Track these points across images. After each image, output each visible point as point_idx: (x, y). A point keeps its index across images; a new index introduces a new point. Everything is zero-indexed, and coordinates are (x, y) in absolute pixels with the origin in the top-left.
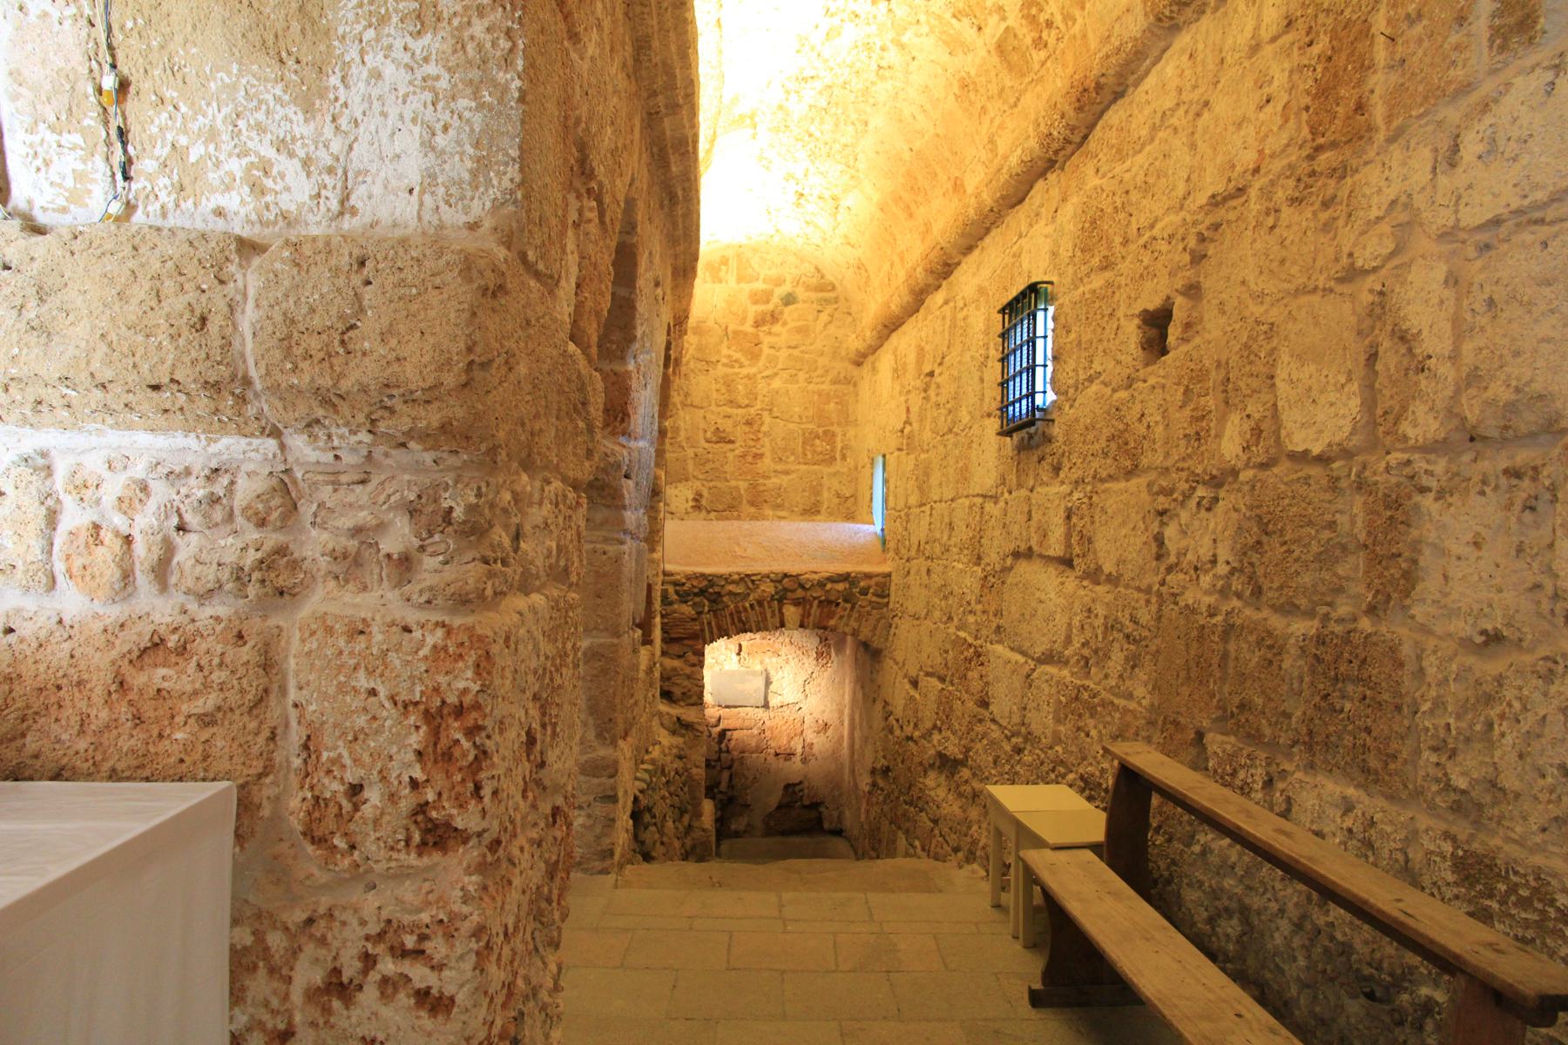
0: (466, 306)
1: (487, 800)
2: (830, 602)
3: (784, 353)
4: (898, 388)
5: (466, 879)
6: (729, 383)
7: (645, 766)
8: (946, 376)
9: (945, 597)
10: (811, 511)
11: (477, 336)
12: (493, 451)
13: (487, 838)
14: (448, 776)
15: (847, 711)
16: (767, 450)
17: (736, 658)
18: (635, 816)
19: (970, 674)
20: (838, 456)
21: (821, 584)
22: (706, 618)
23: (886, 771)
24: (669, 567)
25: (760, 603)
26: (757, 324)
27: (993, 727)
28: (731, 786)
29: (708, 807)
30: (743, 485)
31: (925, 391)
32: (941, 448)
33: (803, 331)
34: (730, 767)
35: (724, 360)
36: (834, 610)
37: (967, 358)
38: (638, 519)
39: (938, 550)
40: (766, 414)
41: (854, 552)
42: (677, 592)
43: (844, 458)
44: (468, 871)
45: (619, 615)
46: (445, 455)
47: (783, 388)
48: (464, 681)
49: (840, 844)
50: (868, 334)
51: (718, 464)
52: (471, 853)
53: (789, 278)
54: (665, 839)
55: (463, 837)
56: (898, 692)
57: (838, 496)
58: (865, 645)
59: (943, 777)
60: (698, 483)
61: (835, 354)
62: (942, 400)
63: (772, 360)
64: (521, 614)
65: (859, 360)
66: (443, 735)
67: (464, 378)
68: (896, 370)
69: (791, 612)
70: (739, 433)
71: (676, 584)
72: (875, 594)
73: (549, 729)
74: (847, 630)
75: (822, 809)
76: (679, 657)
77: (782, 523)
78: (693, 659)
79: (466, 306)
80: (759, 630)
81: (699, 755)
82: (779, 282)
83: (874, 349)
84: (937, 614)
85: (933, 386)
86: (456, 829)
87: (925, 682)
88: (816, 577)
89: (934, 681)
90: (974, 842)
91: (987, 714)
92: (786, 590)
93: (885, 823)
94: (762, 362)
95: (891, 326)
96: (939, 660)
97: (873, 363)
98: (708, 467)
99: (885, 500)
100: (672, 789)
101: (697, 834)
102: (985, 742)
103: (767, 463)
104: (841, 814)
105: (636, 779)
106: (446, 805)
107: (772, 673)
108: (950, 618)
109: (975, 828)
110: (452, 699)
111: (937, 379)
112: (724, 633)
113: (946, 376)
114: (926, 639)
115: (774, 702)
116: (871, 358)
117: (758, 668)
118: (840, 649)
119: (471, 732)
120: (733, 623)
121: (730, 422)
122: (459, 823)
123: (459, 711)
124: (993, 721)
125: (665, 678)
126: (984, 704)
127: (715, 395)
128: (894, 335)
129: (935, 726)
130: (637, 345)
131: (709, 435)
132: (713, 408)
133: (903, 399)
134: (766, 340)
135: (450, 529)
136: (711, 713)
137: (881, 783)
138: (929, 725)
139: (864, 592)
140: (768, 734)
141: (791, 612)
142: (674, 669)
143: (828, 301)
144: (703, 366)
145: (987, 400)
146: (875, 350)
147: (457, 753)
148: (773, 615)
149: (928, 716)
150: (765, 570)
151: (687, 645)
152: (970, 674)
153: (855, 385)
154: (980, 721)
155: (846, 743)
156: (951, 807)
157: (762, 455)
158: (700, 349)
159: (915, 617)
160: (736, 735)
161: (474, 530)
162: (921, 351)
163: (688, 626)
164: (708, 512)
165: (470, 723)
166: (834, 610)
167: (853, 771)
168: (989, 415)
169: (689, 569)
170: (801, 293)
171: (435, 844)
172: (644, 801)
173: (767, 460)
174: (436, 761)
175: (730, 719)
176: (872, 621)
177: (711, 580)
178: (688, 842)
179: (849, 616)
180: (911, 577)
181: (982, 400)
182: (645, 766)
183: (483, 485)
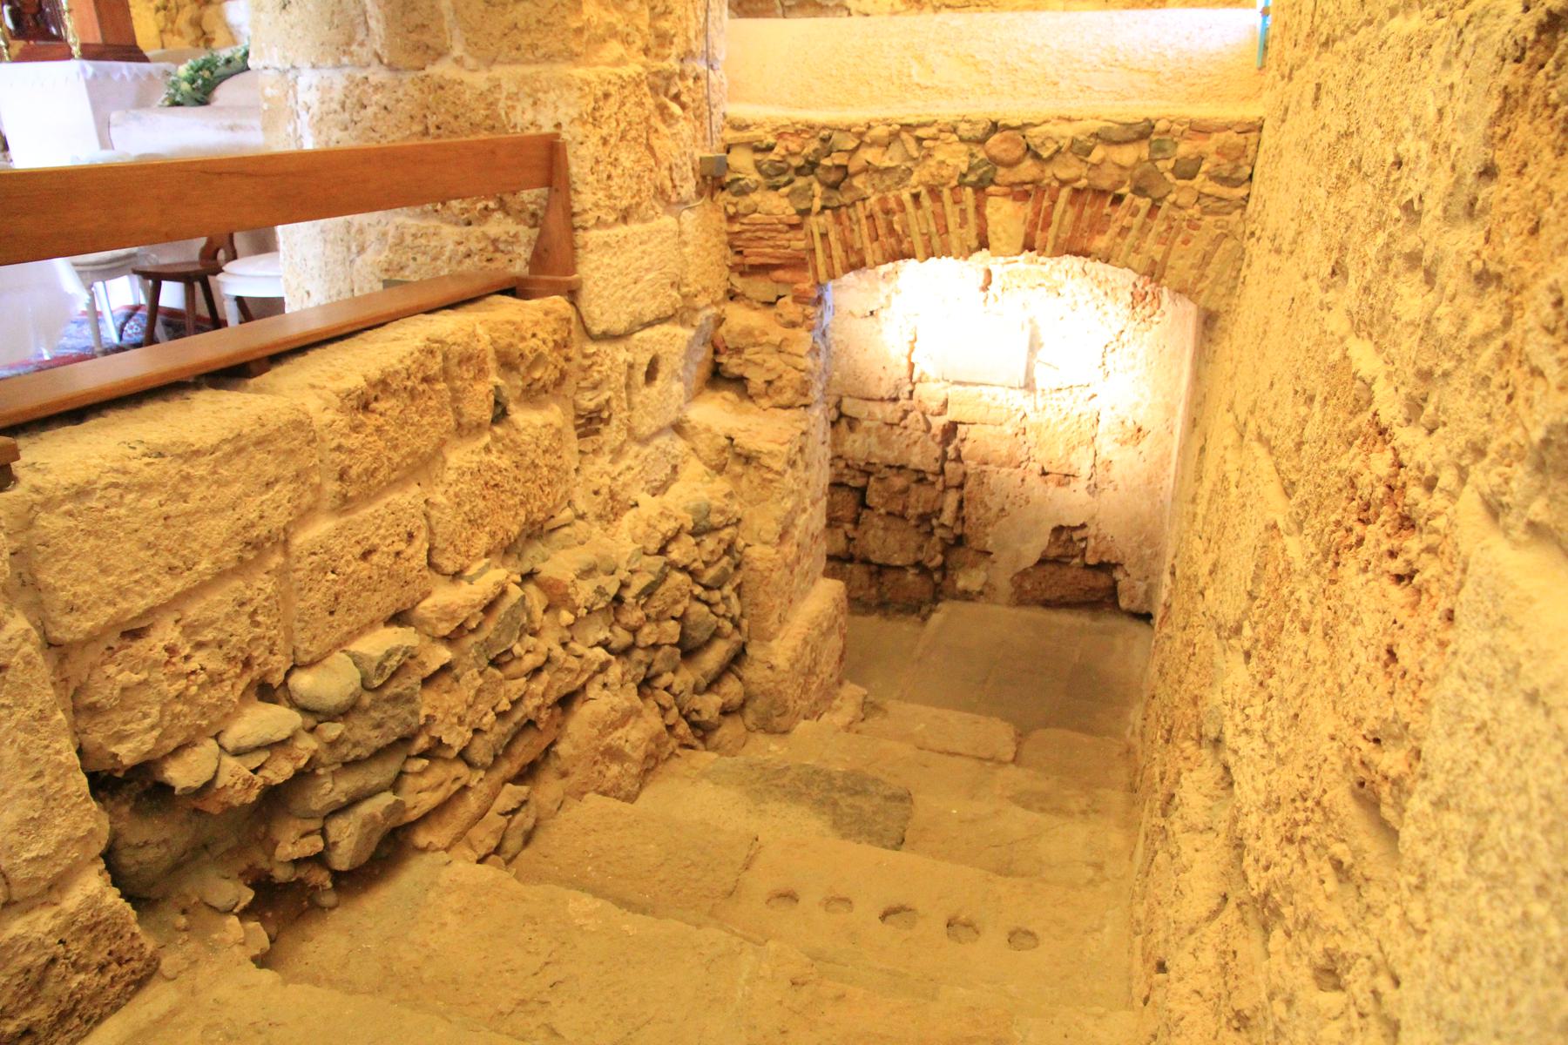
21: (1080, 150)
22: (816, 223)
28: (960, 518)
34: (960, 486)
69: (1004, 214)
75: (1118, 575)
80: (930, 254)
88: (1069, 131)
92: (994, 162)
115: (1042, 379)
120: (875, 238)
139: (1187, 171)
140: (1031, 435)
142: (748, 332)
148: (963, 223)
150: (946, 111)
155: (1172, 470)
163: (782, 240)
176: (1200, 243)
179: (1144, 230)
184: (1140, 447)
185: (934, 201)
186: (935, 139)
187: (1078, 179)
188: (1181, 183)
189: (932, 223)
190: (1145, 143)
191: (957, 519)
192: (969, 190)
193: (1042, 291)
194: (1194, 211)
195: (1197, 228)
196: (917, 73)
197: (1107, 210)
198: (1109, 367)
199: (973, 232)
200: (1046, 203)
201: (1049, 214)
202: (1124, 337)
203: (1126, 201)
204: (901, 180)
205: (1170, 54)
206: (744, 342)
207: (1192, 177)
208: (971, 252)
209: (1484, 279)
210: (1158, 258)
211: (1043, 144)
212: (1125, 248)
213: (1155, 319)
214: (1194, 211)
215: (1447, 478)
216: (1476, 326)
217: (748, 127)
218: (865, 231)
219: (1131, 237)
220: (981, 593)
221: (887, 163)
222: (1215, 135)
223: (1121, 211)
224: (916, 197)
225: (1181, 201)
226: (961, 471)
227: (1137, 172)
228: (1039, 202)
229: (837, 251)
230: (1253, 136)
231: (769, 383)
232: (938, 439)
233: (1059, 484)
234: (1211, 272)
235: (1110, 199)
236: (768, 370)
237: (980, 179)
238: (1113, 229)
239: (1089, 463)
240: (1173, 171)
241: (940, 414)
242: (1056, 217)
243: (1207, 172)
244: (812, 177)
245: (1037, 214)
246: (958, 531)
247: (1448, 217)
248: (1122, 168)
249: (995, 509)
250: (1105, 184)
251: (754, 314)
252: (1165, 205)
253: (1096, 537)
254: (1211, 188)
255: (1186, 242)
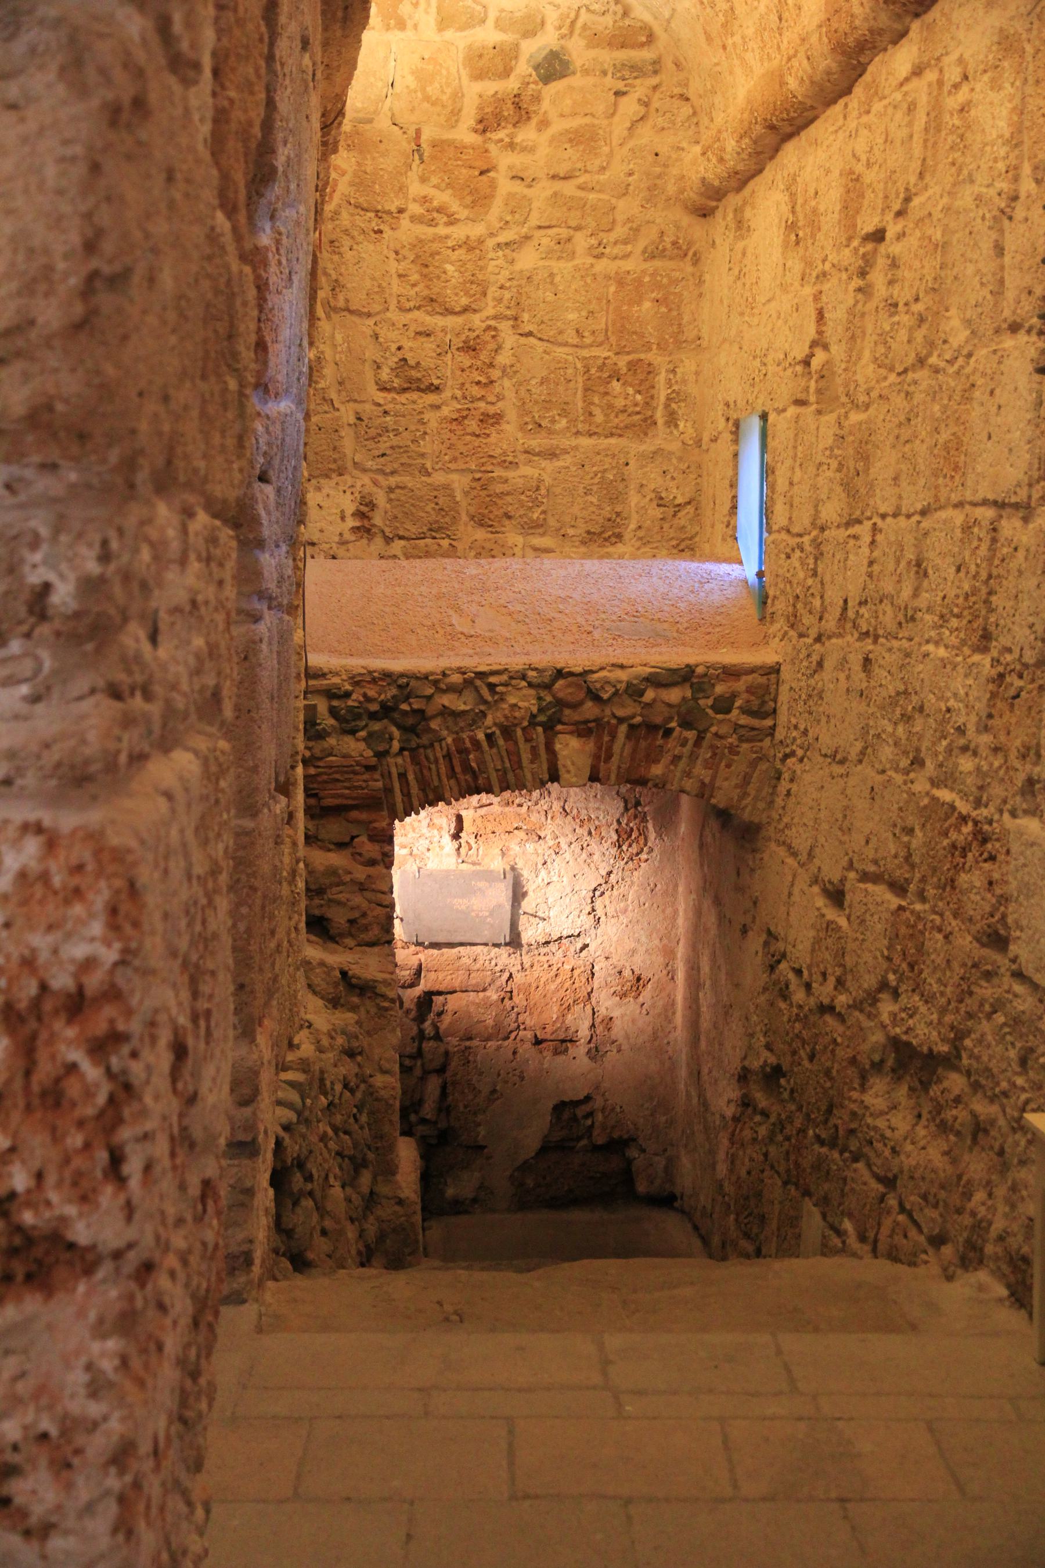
0: (78, 149)
1: (134, 1183)
2: (652, 728)
3: (541, 192)
4: (797, 266)
5: (96, 1347)
6: (425, 260)
7: (290, 1076)
8: (913, 241)
9: (907, 718)
10: (604, 536)
11: (104, 217)
12: (129, 464)
13: (133, 1258)
14: (56, 1136)
15: (681, 951)
16: (509, 407)
17: (449, 845)
18: (278, 1179)
19: (963, 878)
20: (660, 416)
21: (634, 691)
22: (395, 763)
23: (774, 1075)
24: (317, 660)
25: (507, 732)
26: (484, 126)
27: (1018, 988)
28: (444, 1107)
29: (407, 1154)
30: (459, 482)
31: (863, 274)
32: (898, 401)
33: (583, 139)
34: (441, 1070)
35: (415, 208)
36: (658, 746)
37: (966, 198)
38: (280, 566)
39: (888, 617)
40: (505, 326)
41: (700, 623)
42: (333, 712)
43: (672, 420)
44: (100, 1330)
45: (255, 769)
46: (29, 473)
47: (539, 267)
48: (84, 944)
49: (672, 1226)
50: (731, 144)
51: (405, 439)
52: (103, 1293)
53: (552, 17)
54: (328, 1223)
55: (85, 1260)
56: (801, 917)
57: (661, 502)
58: (724, 816)
59: (903, 1090)
60: (366, 479)
61: (653, 192)
62: (902, 294)
63: (517, 206)
64: (169, 796)
65: (707, 204)
66: (42, 1055)
67: (78, 309)
68: (791, 227)
69: (571, 749)
70: (450, 369)
71: (330, 694)
72: (746, 711)
73: (202, 1023)
74: (689, 784)
75: (633, 1153)
76: (341, 846)
77: (547, 563)
78: (371, 850)
79: (78, 149)
80: (505, 787)
81: (388, 1047)
82: (532, 26)
83: (740, 181)
84: (887, 752)
85: (881, 262)
86: (71, 1246)
87: (857, 892)
88: (623, 675)
89: (880, 892)
90: (980, 1227)
91: (1003, 962)
92: (561, 703)
93: (774, 1188)
94: (496, 209)
95: (783, 126)
96: (892, 848)
97: (738, 211)
98: (384, 446)
99: (766, 511)
100: (338, 1119)
101: (386, 1211)
102: (1000, 1018)
103: (510, 435)
104: (671, 1165)
105: (279, 1103)
106: (54, 1196)
107: (525, 873)
108: (918, 762)
109: (980, 1196)
110: (62, 981)
111: (891, 247)
112: (432, 796)
113: (913, 241)
114: (861, 804)
115: (530, 933)
116: (733, 200)
117: (497, 864)
118: (666, 822)
119: (99, 1048)
120: (452, 774)
121: (429, 346)
122: (81, 1233)
123: (76, 1005)
124: (1019, 975)
125: (314, 891)
126: (998, 940)
127: (396, 287)
128: (790, 147)
129: (884, 986)
130: (276, 190)
131: (385, 374)
132: (393, 315)
133: (808, 290)
134: (506, 161)
135: (44, 630)
136: (406, 957)
137: (762, 1100)
138: (870, 981)
139: (724, 706)
140: (519, 999)
141: (571, 749)
142: (332, 871)
143: (636, 70)
144: (366, 221)
145: (1010, 295)
146: (744, 183)
147: (73, 1088)
149: (869, 961)
150: (516, 662)
151: (356, 817)
152: (963, 878)
153: (696, 261)
154: (988, 975)
155: (679, 1019)
156: (924, 1152)
157: (497, 418)
158: (361, 182)
159: (836, 757)
160: (453, 1003)
161: (91, 630)
162: (854, 186)
164: (388, 540)
165: (99, 1026)
166: (658, 746)
167: (696, 1075)
168: (1014, 328)
169: (357, 663)
170: (578, 52)
171: (29, 1277)
172: (293, 1148)
173: (510, 427)
174: (29, 1108)
175: (441, 970)
176: (740, 766)
177: (404, 684)
178: (371, 1228)
179: (693, 757)
180: (827, 674)
181: (998, 292)
182: (290, 1076)
183: (112, 534)
184: (641, 999)
185: (506, 740)
186: (506, 685)
187: (633, 717)
188: (720, 717)
189: (507, 761)
190: (688, 685)
191: (440, 1110)
192: (540, 729)
193: (521, 834)
194: (732, 740)
195: (737, 753)
196: (460, 624)
197: (660, 742)
198: (600, 912)
199: (545, 767)
200: (606, 738)
201: (609, 749)
202: (613, 878)
203: (675, 734)
204: (474, 722)
205: (682, 605)
206: (327, 881)
207: (728, 711)
208: (543, 784)
209: (996, 750)
210: (707, 780)
211: (602, 687)
212: (678, 774)
213: (644, 856)
214: (732, 740)
215: (996, 817)
216: (996, 764)
217: (324, 675)
218: (443, 770)
219: (682, 764)
220: (474, 1200)
221: (463, 707)
222: (744, 678)
223: (671, 743)
224: (489, 737)
225: (721, 732)
226: (442, 1050)
227: (683, 709)
228: (599, 738)
229: (415, 790)
230: (773, 676)
231: (352, 922)
232: (413, 1014)
233: (556, 1053)
234: (752, 789)
235: (661, 733)
236: (352, 909)
237: (550, 719)
238: (666, 759)
239: (587, 1023)
240: (712, 707)
241: (412, 985)
242: (617, 748)
243: (740, 708)
244: (385, 721)
245: (600, 748)
246: (442, 1125)
247: (978, 731)
248: (669, 705)
249: (485, 1090)
250: (658, 720)
251: (331, 855)
252: (709, 735)
253: (603, 1110)
254: (744, 720)
255: (728, 766)
